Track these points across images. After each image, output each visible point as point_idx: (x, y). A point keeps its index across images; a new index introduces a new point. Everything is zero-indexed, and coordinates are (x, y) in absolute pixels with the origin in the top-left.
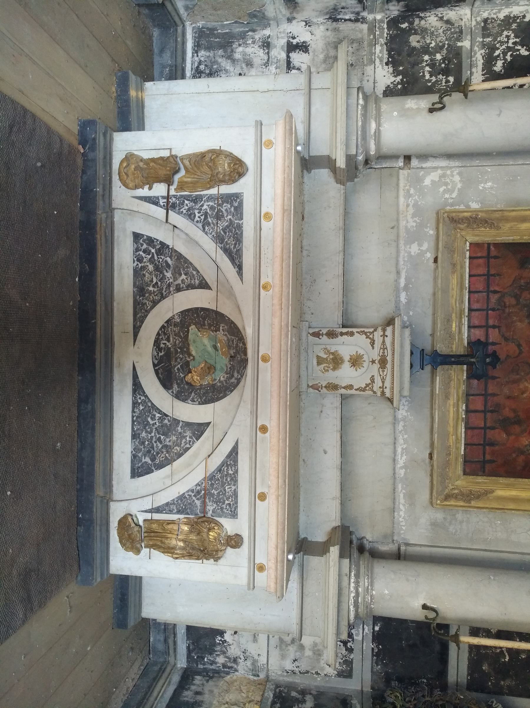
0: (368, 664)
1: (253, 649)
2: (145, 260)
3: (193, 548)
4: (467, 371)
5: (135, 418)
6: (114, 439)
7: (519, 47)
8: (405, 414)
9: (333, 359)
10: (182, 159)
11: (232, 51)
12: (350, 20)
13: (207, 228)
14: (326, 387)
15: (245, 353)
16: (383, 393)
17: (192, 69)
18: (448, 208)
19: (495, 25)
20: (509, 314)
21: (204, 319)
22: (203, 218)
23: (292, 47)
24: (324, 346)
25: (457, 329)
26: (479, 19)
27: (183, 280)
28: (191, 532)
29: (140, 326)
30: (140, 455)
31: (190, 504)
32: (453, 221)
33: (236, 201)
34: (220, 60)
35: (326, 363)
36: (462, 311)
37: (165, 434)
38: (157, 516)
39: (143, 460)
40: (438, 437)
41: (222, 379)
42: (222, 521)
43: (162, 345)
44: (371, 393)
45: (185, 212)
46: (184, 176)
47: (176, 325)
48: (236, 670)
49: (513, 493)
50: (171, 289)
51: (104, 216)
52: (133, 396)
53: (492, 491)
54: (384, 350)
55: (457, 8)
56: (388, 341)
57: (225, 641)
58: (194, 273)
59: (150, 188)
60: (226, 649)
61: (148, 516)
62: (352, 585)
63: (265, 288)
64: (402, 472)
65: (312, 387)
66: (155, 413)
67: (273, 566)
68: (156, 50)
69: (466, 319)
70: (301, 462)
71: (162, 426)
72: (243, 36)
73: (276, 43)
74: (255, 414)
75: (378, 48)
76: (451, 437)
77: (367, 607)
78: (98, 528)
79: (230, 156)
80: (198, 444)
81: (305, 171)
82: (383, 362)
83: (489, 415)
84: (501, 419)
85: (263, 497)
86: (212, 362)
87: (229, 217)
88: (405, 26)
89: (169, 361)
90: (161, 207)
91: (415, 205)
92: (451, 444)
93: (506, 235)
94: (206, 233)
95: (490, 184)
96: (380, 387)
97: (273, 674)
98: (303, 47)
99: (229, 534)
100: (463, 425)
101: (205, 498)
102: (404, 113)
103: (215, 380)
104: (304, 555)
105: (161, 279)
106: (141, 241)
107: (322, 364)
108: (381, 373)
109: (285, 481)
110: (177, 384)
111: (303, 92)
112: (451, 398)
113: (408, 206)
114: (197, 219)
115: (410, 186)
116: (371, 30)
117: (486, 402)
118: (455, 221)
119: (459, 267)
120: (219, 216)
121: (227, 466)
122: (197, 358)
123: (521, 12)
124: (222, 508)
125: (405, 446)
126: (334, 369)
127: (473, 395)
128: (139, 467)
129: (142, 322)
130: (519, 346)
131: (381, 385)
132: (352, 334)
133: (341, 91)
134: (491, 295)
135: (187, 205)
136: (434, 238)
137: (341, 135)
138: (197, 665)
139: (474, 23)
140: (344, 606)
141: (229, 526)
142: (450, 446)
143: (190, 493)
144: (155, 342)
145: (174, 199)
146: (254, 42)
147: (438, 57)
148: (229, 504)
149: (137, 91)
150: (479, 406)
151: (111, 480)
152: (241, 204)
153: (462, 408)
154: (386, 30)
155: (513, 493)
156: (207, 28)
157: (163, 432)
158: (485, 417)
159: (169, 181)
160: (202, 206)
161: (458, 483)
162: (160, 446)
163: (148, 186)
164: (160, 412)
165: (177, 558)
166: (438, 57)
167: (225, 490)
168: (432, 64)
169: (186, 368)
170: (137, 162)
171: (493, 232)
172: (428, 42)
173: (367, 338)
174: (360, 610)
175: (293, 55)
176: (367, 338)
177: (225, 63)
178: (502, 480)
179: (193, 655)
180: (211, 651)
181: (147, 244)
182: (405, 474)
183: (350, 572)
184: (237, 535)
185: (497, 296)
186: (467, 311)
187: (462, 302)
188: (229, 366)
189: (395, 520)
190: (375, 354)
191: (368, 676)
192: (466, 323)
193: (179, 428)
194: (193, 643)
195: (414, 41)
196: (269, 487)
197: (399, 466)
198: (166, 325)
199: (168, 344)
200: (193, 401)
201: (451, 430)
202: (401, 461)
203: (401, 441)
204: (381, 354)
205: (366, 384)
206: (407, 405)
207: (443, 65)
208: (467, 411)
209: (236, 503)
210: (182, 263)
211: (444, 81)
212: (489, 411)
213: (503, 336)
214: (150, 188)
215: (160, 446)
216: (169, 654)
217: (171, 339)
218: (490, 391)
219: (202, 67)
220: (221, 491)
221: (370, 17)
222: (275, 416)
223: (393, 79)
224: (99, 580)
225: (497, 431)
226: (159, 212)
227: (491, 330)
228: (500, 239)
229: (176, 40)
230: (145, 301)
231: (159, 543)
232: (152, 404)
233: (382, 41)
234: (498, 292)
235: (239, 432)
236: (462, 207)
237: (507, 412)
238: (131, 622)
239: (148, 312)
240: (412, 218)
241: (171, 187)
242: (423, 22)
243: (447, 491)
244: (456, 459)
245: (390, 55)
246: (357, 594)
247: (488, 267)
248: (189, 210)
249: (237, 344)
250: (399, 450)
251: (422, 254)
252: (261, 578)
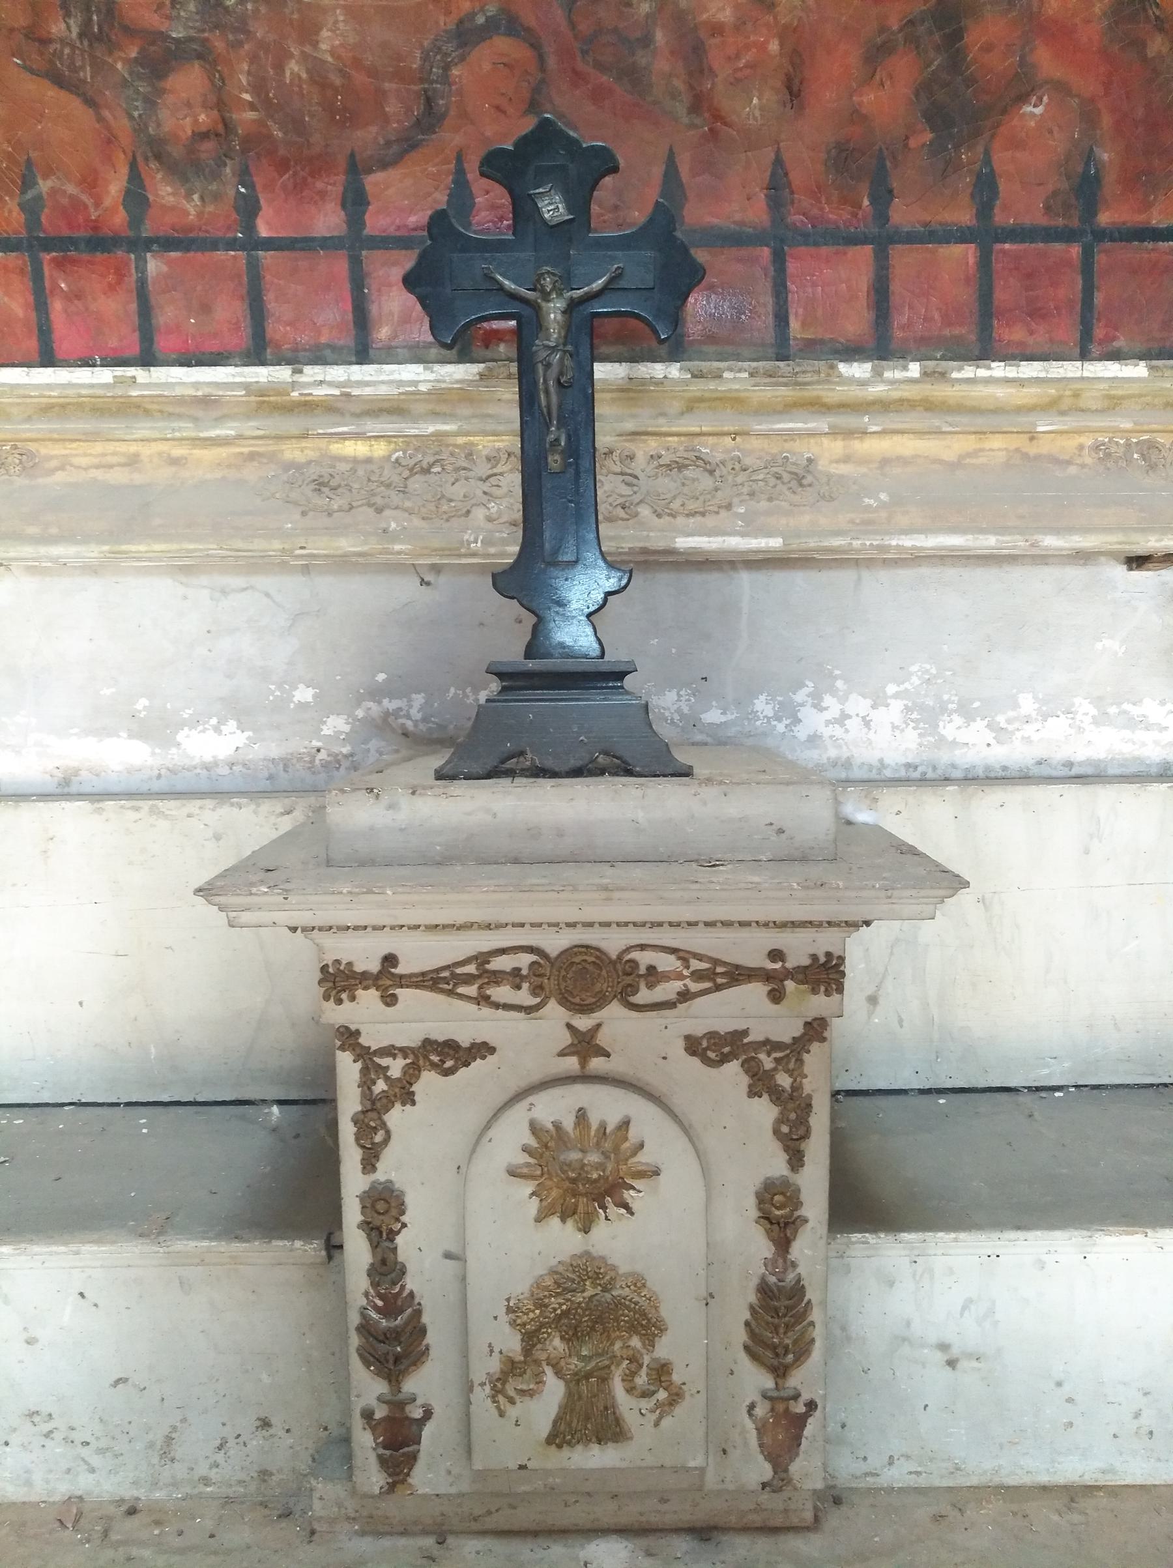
4: (633, 359)
9: (573, 1336)
20: (264, 103)
24: (481, 1395)
25: (373, 426)
35: (604, 1380)
36: (267, 403)
40: (1057, 531)
54: (496, 978)
69: (312, 373)
76: (1044, 447)
82: (586, 979)
83: (903, 215)
84: (928, 136)
92: (1087, 440)
96: (776, 996)
100: (969, 371)
107: (610, 1408)
108: (667, 990)
112: (804, 449)
125: (1085, 708)
126: (648, 1325)
127: (782, 319)
130: (466, 35)
131: (756, 991)
132: (385, 1209)
142: (1096, 448)
153: (863, 383)
158: (911, 238)
173: (409, 1098)
176: (409, 1098)
186: (261, 374)
190: (531, 1036)
192: (337, 373)
204: (524, 997)
205: (753, 1093)
206: (843, 700)
212: (882, 216)
225: (1002, 159)
234: (135, 176)
237: (889, 100)
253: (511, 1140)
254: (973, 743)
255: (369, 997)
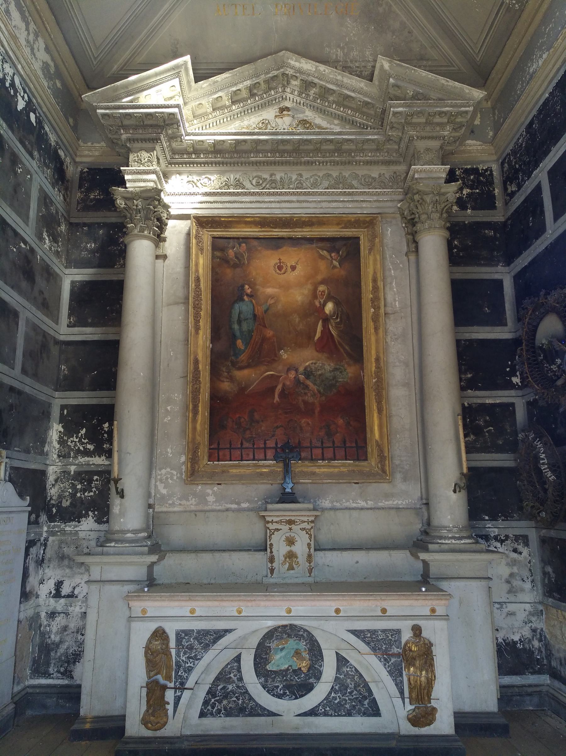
0: (514, 524)
1: (521, 616)
2: (219, 707)
3: (426, 663)
5: (336, 714)
6: (353, 732)
7: (80, 434)
8: (328, 501)
10: (149, 677)
11: (53, 644)
12: (44, 550)
13: (199, 657)
14: (310, 563)
15: (285, 626)
16: (312, 522)
17: (62, 679)
18: (183, 476)
19: (63, 450)
21: (262, 658)
22: (191, 660)
23: (58, 594)
24: (280, 565)
26: (57, 461)
27: (235, 676)
28: (414, 665)
29: (268, 710)
30: (363, 709)
31: (394, 667)
32: (193, 474)
33: (181, 635)
34: (59, 654)
37: (347, 687)
38: (407, 694)
39: (367, 706)
41: (304, 644)
42: (403, 641)
43: (282, 692)
44: (312, 530)
45: (186, 675)
46: (162, 676)
47: (266, 681)
48: (542, 630)
49: (376, 428)
50: (241, 685)
51: (186, 743)
52: (319, 716)
53: (377, 441)
55: (48, 475)
56: (275, 519)
57: (520, 640)
58: (229, 666)
59: (168, 703)
60: (526, 639)
61: (407, 701)
62: (447, 542)
63: (240, 612)
64: (370, 502)
65: (310, 574)
66: (331, 697)
67: (430, 602)
68: (44, 712)
69: (260, 462)
70: (366, 580)
71: (341, 691)
72: (43, 635)
73: (52, 607)
74: (327, 618)
75: (67, 529)
77: (461, 530)
78: (420, 744)
79: (150, 641)
80: (352, 662)
81: (155, 582)
82: (290, 522)
85: (384, 611)
86: (293, 652)
87: (192, 640)
88: (54, 510)
89: (293, 685)
90: (182, 694)
91: (180, 499)
93: (203, 438)
94: (202, 657)
95: (169, 450)
97: (538, 598)
98: (59, 585)
99: (412, 635)
101: (389, 655)
102: (122, 514)
103: (305, 649)
104: (430, 578)
105: (233, 693)
106: (206, 711)
107: (293, 566)
108: (298, 523)
109: (371, 595)
110: (309, 679)
111: (102, 586)
113: (180, 504)
114: (191, 665)
115: (167, 503)
116: (53, 534)
117: (316, 447)
118: (193, 472)
119: (225, 469)
120: (191, 648)
121: (365, 638)
122: (290, 664)
123: (57, 434)
124: (395, 641)
125: (351, 501)
126: (297, 557)
127: (312, 456)
128: (372, 710)
129: (265, 709)
132: (271, 545)
133: (105, 559)
134: (244, 446)
135: (182, 673)
136: (204, 485)
137: (136, 559)
138: (545, 665)
139: (60, 464)
140: (462, 546)
141: (407, 635)
143: (387, 666)
144: (279, 698)
145: (177, 683)
146: (49, 625)
147: (79, 487)
148: (392, 635)
149: (86, 723)
150: (318, 452)
151: (383, 734)
152: (183, 631)
154: (56, 523)
155: (376, 428)
156: (33, 665)
157: (345, 689)
158: (326, 447)
159: (164, 688)
160: (183, 661)
161: (373, 464)
162: (355, 692)
163: (166, 705)
164: (330, 693)
165: (435, 677)
166: (79, 487)
167: (382, 639)
168: (84, 491)
169: (297, 672)
170: (149, 714)
171: (201, 447)
172: (68, 494)
174: (465, 535)
175: (63, 593)
177: (61, 650)
178: (368, 435)
179: (537, 669)
180: (530, 653)
181: (208, 706)
182: (371, 501)
183: (438, 543)
184: (412, 630)
185: (244, 443)
187: (248, 465)
188: (295, 638)
189: (405, 507)
191: (523, 523)
192: (263, 462)
193: (341, 677)
194: (527, 669)
195: (66, 503)
196: (376, 606)
197: (366, 505)
198: (266, 689)
199: (280, 688)
200: (321, 666)
201: (336, 470)
202: (362, 504)
203: (347, 504)
207: (85, 483)
208: (323, 459)
209: (390, 630)
210: (223, 677)
211: (96, 482)
213: (271, 437)
214: (168, 703)
215: (355, 692)
216: (540, 691)
217: (277, 684)
218: (309, 445)
219: (62, 670)
220: (383, 642)
221: (45, 535)
222: (328, 603)
223: (90, 517)
224: (460, 743)
226: (186, 694)
227: (268, 446)
228: (207, 443)
229: (38, 693)
230: (249, 707)
231: (426, 691)
232: (324, 699)
233: (63, 526)
235: (340, 629)
236: (184, 467)
238: (502, 721)
239: (257, 704)
240: (189, 501)
241: (168, 686)
242: (54, 498)
243: (380, 472)
244: (357, 466)
245: (74, 520)
246: (453, 538)
247: (225, 449)
248: (185, 671)
249: (279, 632)
250: (354, 505)
251: (214, 493)
252: (440, 611)
253: (284, 538)
254: (338, 505)
255: (271, 524)
